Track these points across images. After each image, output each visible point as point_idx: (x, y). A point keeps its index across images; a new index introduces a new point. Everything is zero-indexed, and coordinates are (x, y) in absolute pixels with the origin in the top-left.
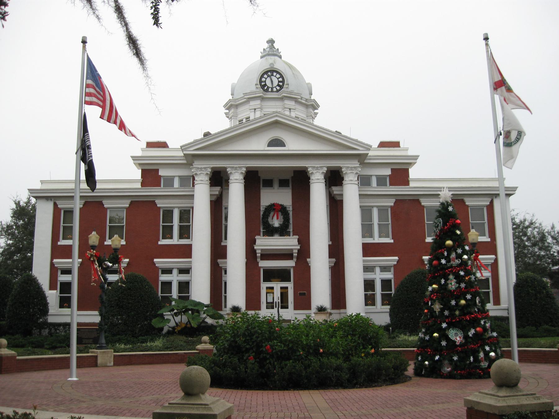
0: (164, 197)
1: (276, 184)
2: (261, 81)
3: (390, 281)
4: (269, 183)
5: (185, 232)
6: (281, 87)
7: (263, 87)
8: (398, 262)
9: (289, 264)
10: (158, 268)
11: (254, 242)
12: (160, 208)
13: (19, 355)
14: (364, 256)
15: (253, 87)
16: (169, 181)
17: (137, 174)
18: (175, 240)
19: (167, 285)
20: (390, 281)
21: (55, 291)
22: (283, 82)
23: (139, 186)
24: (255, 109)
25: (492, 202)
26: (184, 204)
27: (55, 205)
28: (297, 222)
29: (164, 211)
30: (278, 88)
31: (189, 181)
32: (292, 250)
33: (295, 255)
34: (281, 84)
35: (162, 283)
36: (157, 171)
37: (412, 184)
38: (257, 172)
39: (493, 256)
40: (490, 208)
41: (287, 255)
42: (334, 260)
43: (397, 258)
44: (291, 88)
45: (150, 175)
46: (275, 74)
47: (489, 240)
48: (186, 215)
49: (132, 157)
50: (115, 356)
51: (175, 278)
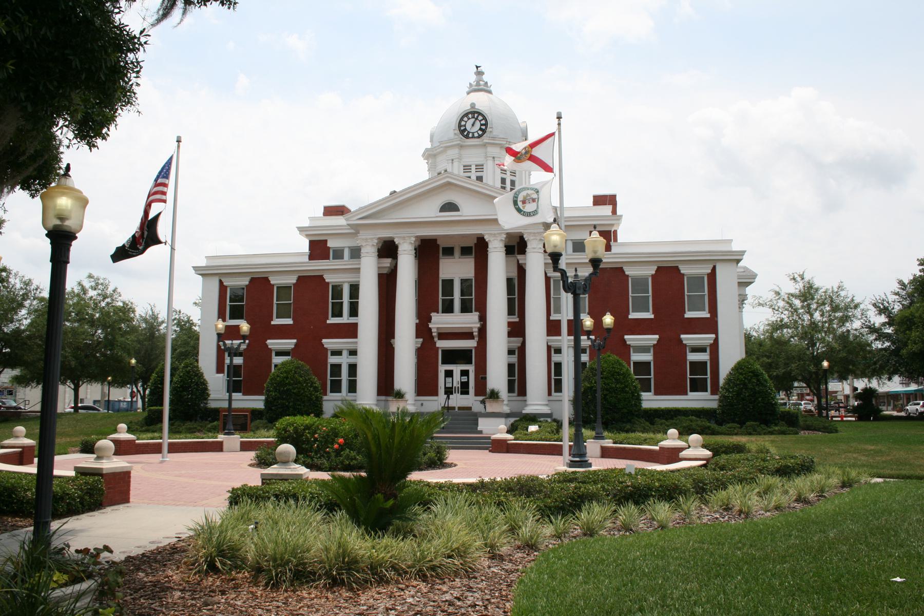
0: (333, 272)
1: (457, 252)
2: (460, 126)
3: (650, 363)
4: (449, 252)
5: (354, 312)
6: (484, 131)
7: (462, 132)
8: (659, 341)
9: (470, 344)
10: (271, 350)
11: (429, 319)
13: (138, 439)
14: (548, 335)
15: (452, 132)
16: (338, 254)
17: (304, 246)
18: (345, 319)
19: (337, 368)
20: (650, 363)
21: (221, 375)
22: (486, 125)
23: (306, 259)
25: (714, 269)
26: (351, 278)
27: (221, 282)
28: (474, 296)
29: (333, 286)
30: (480, 132)
31: (356, 253)
32: (471, 328)
33: (476, 334)
34: (483, 127)
35: (332, 365)
36: (326, 241)
38: (436, 240)
39: (713, 336)
40: (712, 276)
41: (468, 335)
42: (421, 340)
43: (657, 336)
44: (495, 133)
45: (319, 249)
47: (708, 316)
48: (355, 290)
49: (299, 228)
50: (242, 442)
51: (344, 360)
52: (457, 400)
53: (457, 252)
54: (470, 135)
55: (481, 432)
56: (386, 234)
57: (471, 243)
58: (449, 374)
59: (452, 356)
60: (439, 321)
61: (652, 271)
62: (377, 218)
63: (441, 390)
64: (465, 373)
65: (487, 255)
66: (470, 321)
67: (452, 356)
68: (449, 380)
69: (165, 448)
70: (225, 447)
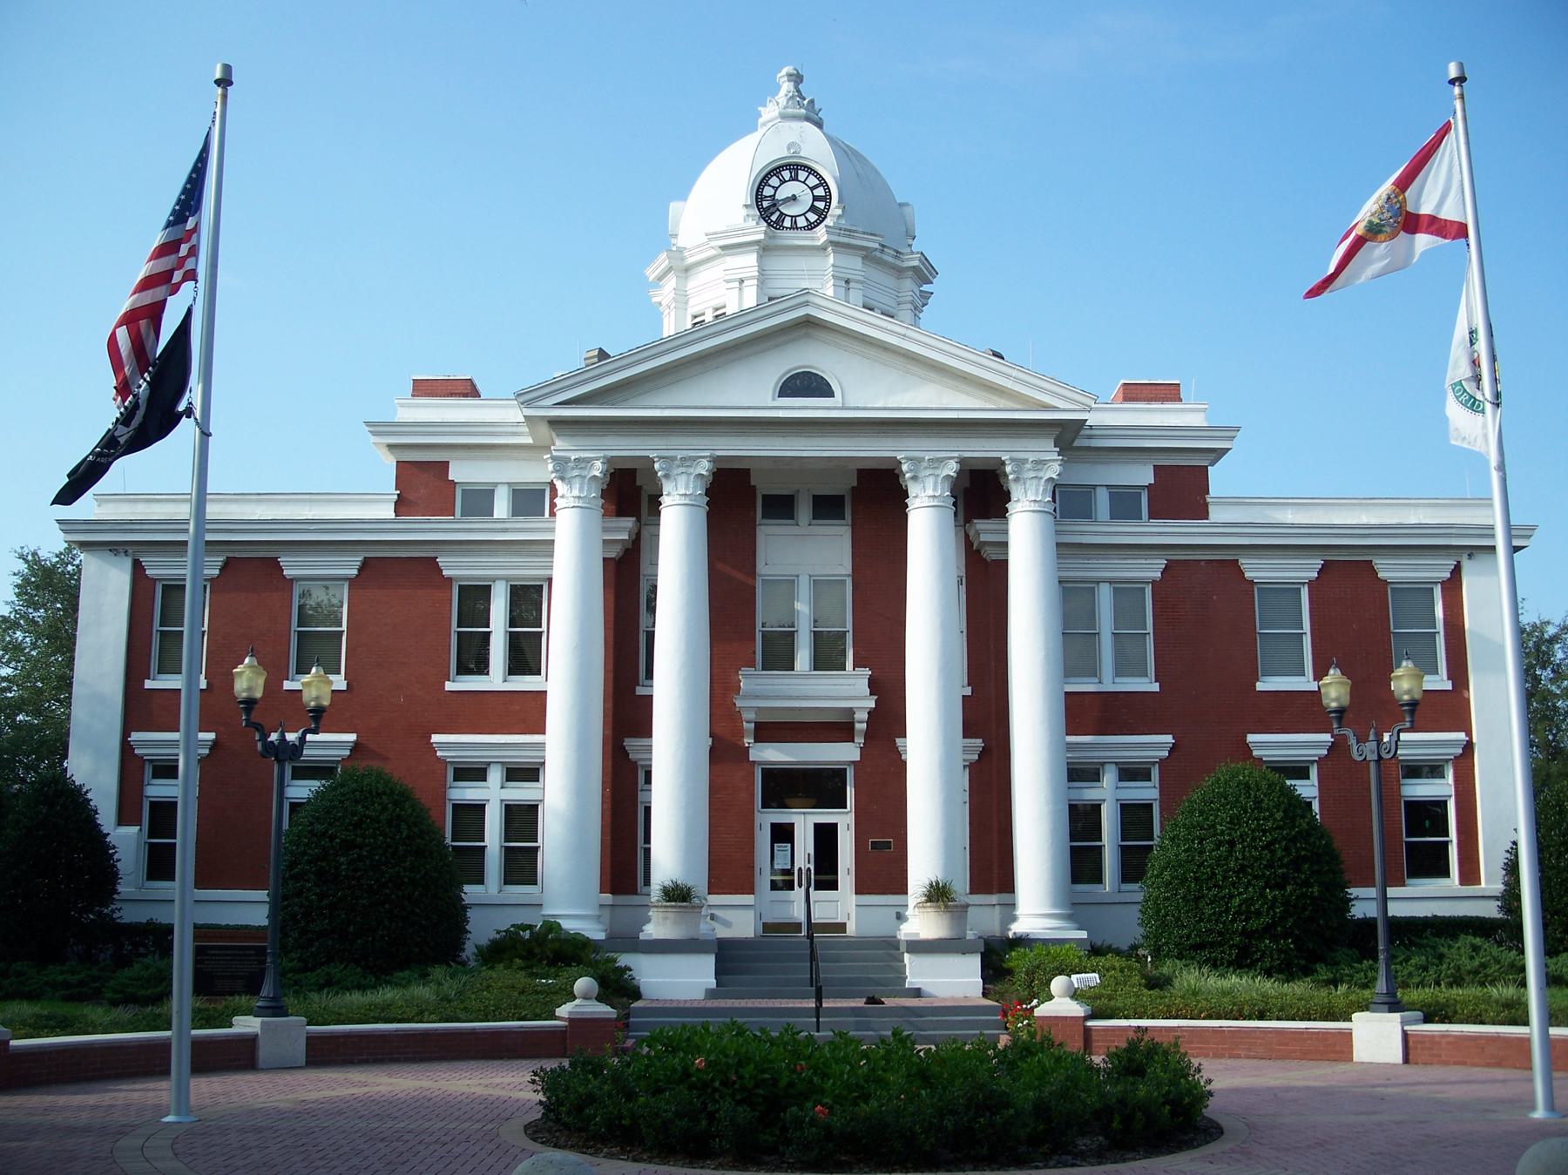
0: (470, 553)
1: (804, 510)
3: (1443, 804)
4: (781, 507)
5: (525, 656)
9: (844, 753)
12: (450, 579)
16: (480, 501)
17: (383, 476)
18: (496, 679)
19: (472, 814)
23: (388, 512)
24: (742, 281)
25: (1457, 571)
30: (813, 217)
32: (851, 711)
33: (861, 727)
34: (821, 205)
35: (152, 804)
36: (444, 466)
37: (1216, 514)
38: (747, 472)
39: (1462, 736)
41: (839, 729)
45: (423, 481)
46: (802, 175)
47: (1448, 686)
48: (528, 601)
50: (312, 1041)
52: (794, 905)
53: (804, 510)
54: (787, 223)
55: (917, 993)
56: (628, 448)
57: (842, 486)
58: (783, 834)
59: (789, 787)
60: (762, 691)
61: (1309, 569)
62: (613, 405)
63: (764, 878)
64: (826, 837)
65: (906, 516)
66: (849, 690)
67: (789, 787)
68: (782, 849)
69: (180, 1059)
70: (264, 1052)
